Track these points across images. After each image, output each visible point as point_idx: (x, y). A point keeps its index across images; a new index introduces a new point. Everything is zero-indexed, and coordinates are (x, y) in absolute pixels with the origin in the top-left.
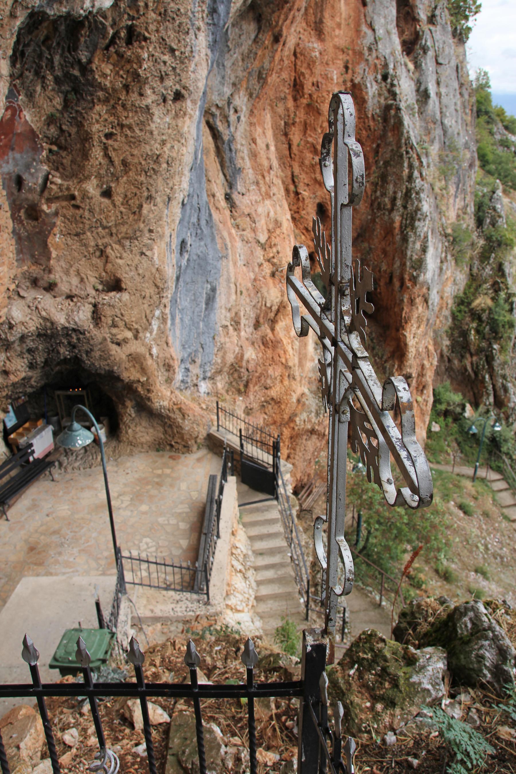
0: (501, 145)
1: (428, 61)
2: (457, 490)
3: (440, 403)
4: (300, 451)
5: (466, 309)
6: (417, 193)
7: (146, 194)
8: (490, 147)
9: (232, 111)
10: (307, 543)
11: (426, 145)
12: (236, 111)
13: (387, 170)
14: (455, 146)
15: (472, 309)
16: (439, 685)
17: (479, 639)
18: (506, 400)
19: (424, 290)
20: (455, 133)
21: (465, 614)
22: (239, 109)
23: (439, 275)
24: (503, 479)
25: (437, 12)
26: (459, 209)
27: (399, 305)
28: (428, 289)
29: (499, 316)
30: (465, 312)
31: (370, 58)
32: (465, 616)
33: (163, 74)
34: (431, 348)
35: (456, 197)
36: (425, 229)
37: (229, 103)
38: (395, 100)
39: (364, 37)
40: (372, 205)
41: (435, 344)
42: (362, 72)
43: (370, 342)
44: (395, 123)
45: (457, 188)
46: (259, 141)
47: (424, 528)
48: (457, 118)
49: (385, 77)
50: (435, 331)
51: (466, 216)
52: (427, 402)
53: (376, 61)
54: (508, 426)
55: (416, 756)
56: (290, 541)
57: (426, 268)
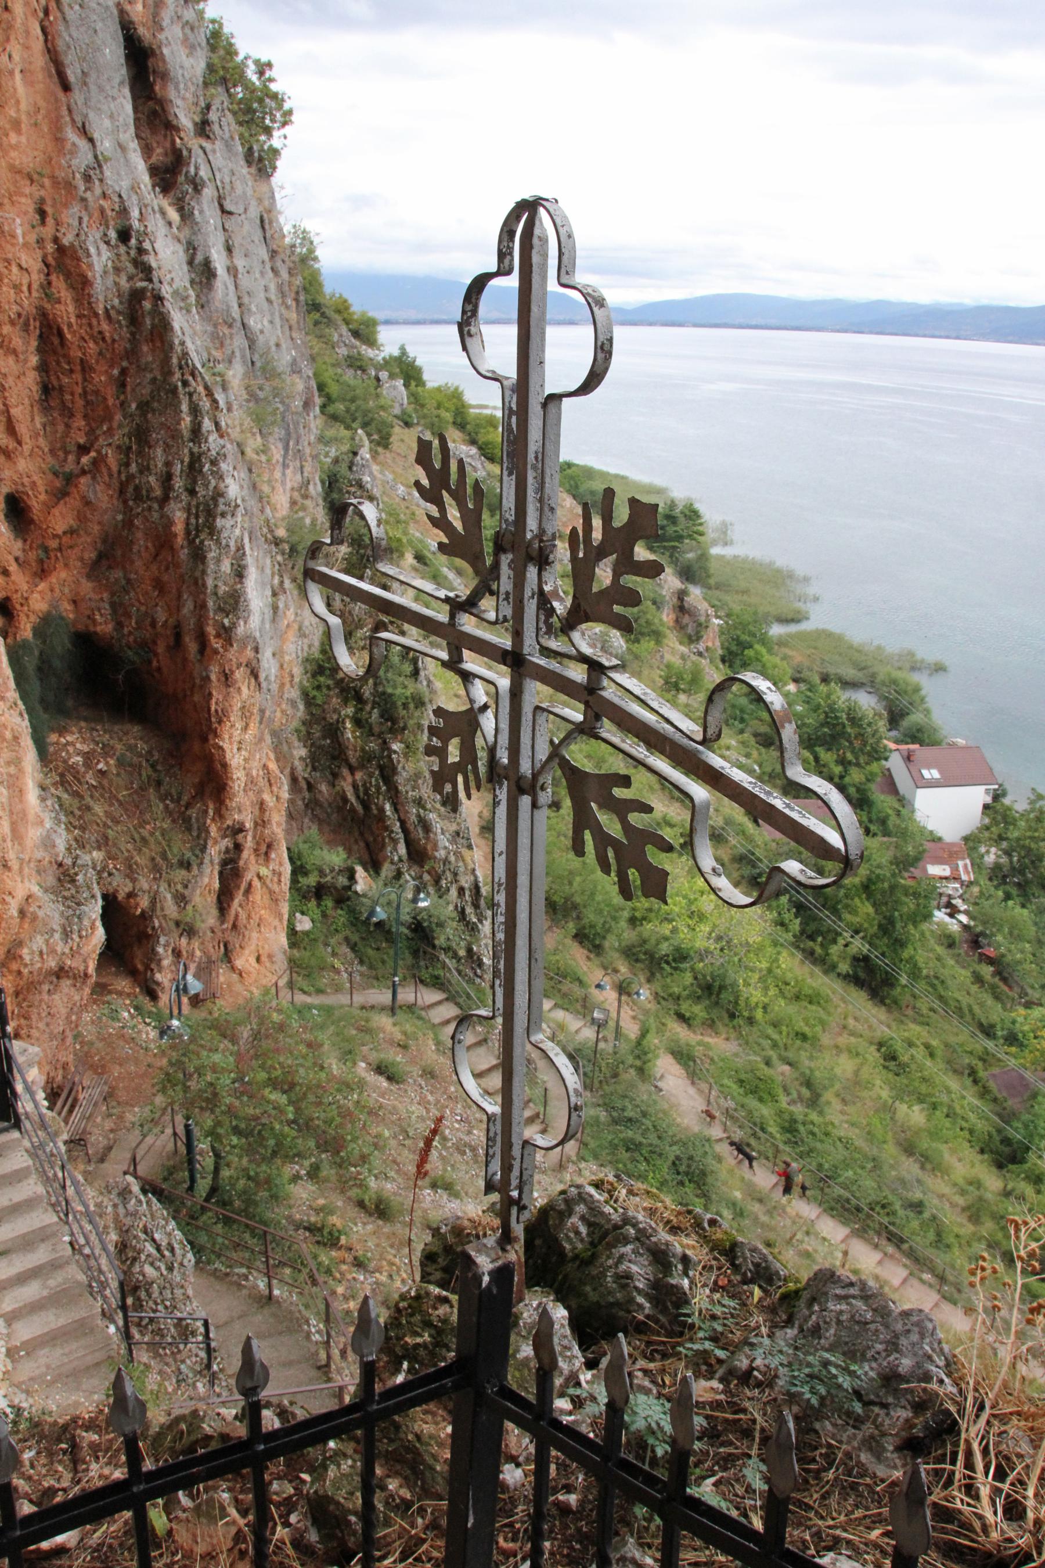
0: (350, 366)
1: (205, 207)
2: (368, 1037)
3: (306, 874)
4: (41, 1019)
5: (330, 682)
6: (214, 463)
8: (331, 371)
10: (98, 1205)
11: (220, 368)
13: (147, 421)
14: (274, 369)
15: (342, 680)
16: (570, 1349)
17: (611, 1246)
18: (429, 847)
19: (249, 653)
20: (272, 343)
21: (570, 1212)
23: (274, 620)
24: (447, 999)
25: (213, 116)
26: (292, 489)
27: (201, 687)
28: (257, 650)
29: (395, 687)
30: (328, 688)
31: (88, 195)
32: (570, 1216)
34: (273, 766)
35: (285, 466)
36: (237, 532)
38: (150, 280)
39: (71, 153)
40: (122, 492)
41: (278, 760)
42: (76, 223)
43: (150, 771)
44: (153, 326)
45: (286, 448)
47: (328, 1122)
48: (272, 314)
49: (124, 235)
50: (274, 734)
51: (308, 503)
52: (280, 874)
53: (101, 202)
54: (440, 897)
55: (569, 1489)
56: (65, 1211)
57: (247, 609)
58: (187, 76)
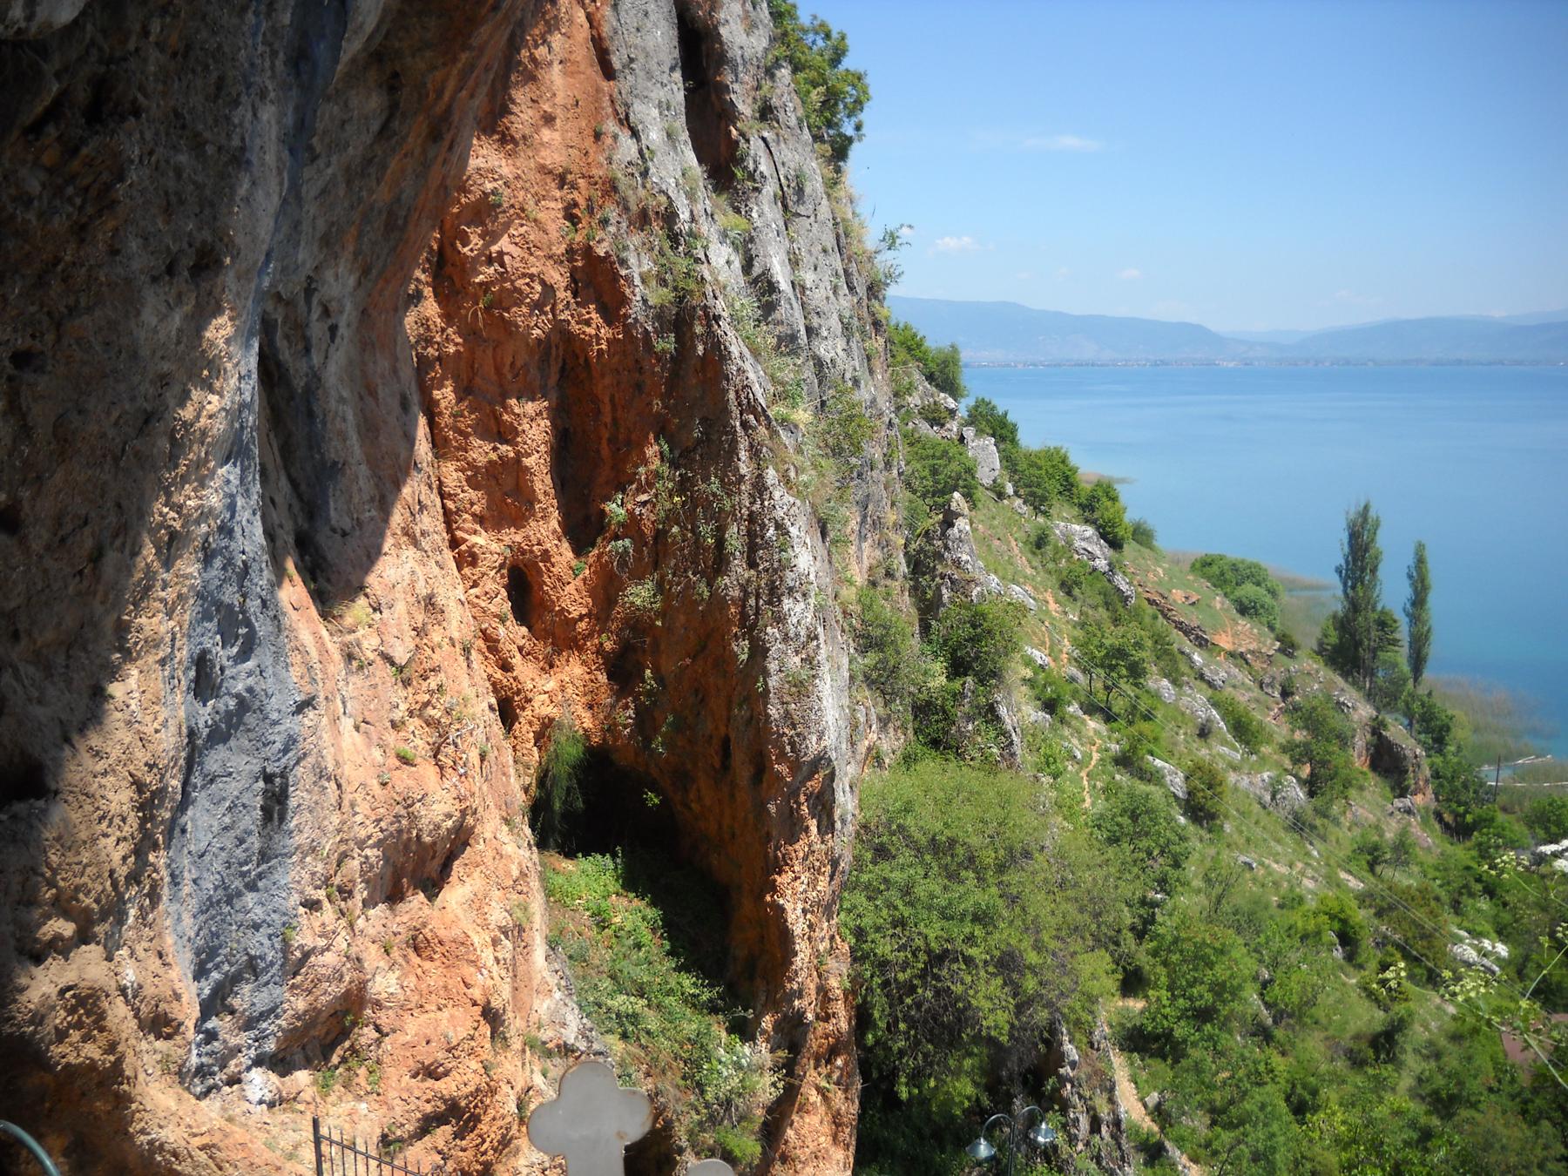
1: (766, 208)
7: (112, 519)
9: (316, 313)
12: (326, 312)
22: (333, 306)
33: (173, 199)
37: (309, 292)
46: (382, 392)
58: (747, 56)
